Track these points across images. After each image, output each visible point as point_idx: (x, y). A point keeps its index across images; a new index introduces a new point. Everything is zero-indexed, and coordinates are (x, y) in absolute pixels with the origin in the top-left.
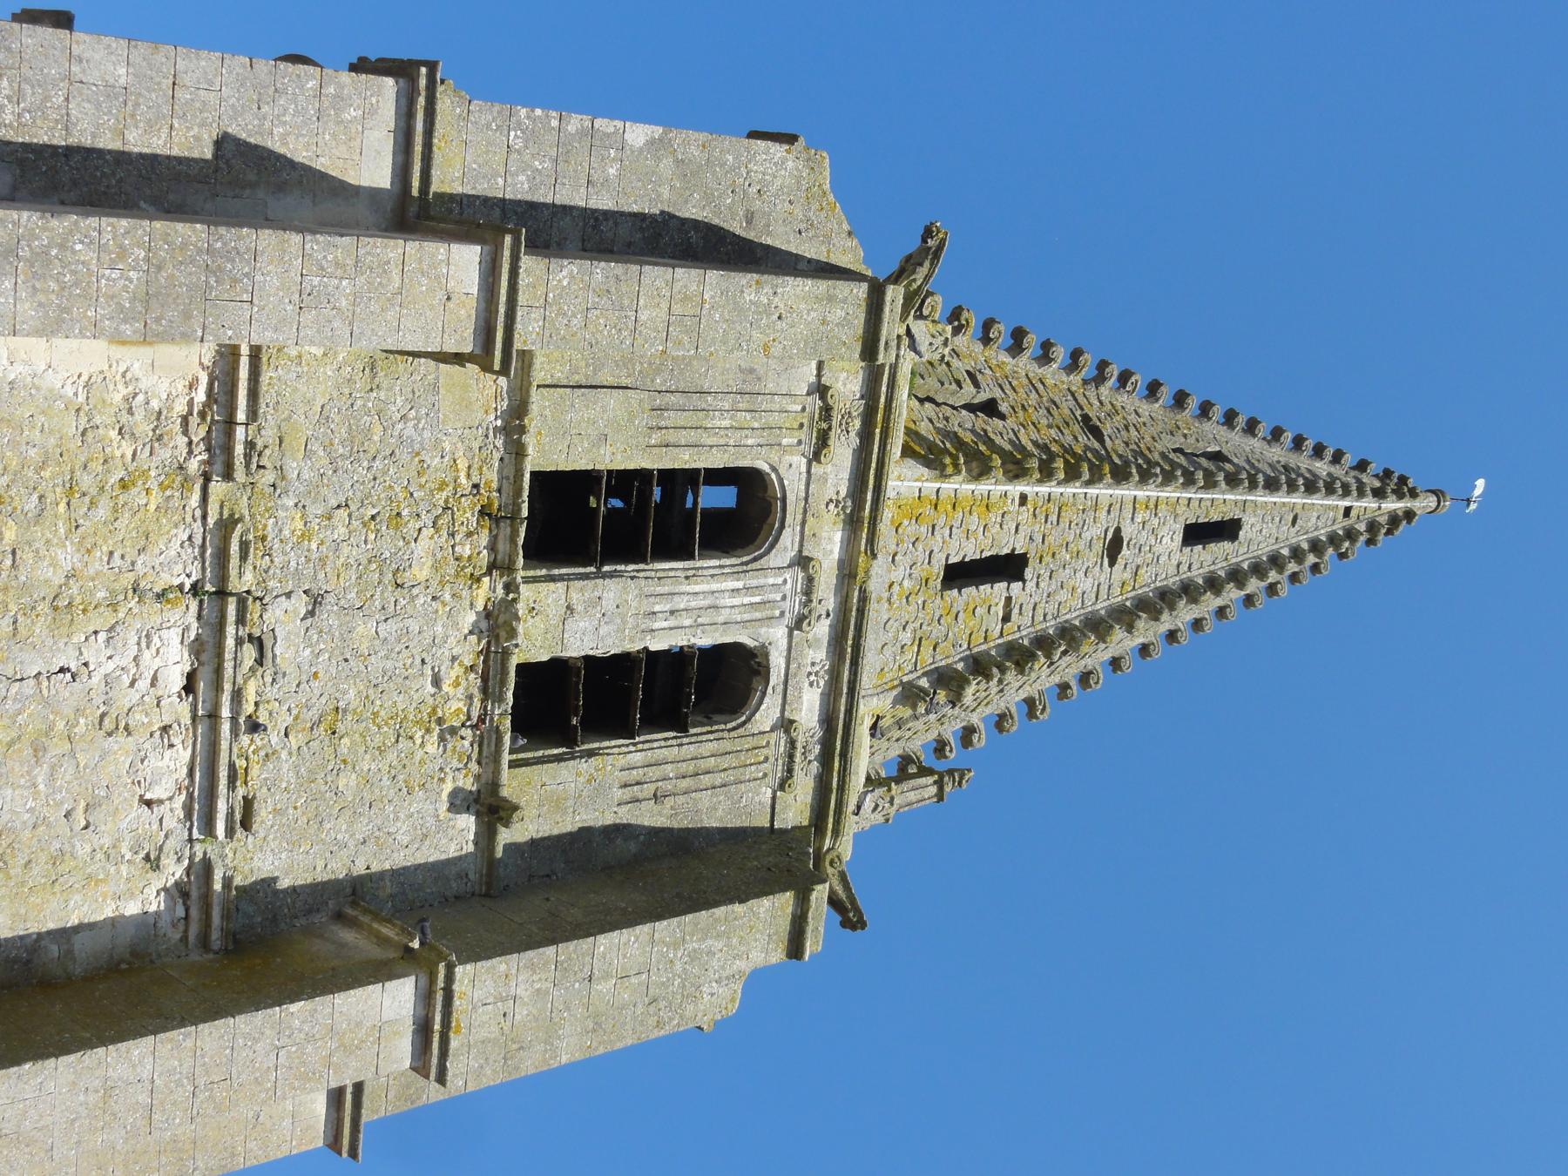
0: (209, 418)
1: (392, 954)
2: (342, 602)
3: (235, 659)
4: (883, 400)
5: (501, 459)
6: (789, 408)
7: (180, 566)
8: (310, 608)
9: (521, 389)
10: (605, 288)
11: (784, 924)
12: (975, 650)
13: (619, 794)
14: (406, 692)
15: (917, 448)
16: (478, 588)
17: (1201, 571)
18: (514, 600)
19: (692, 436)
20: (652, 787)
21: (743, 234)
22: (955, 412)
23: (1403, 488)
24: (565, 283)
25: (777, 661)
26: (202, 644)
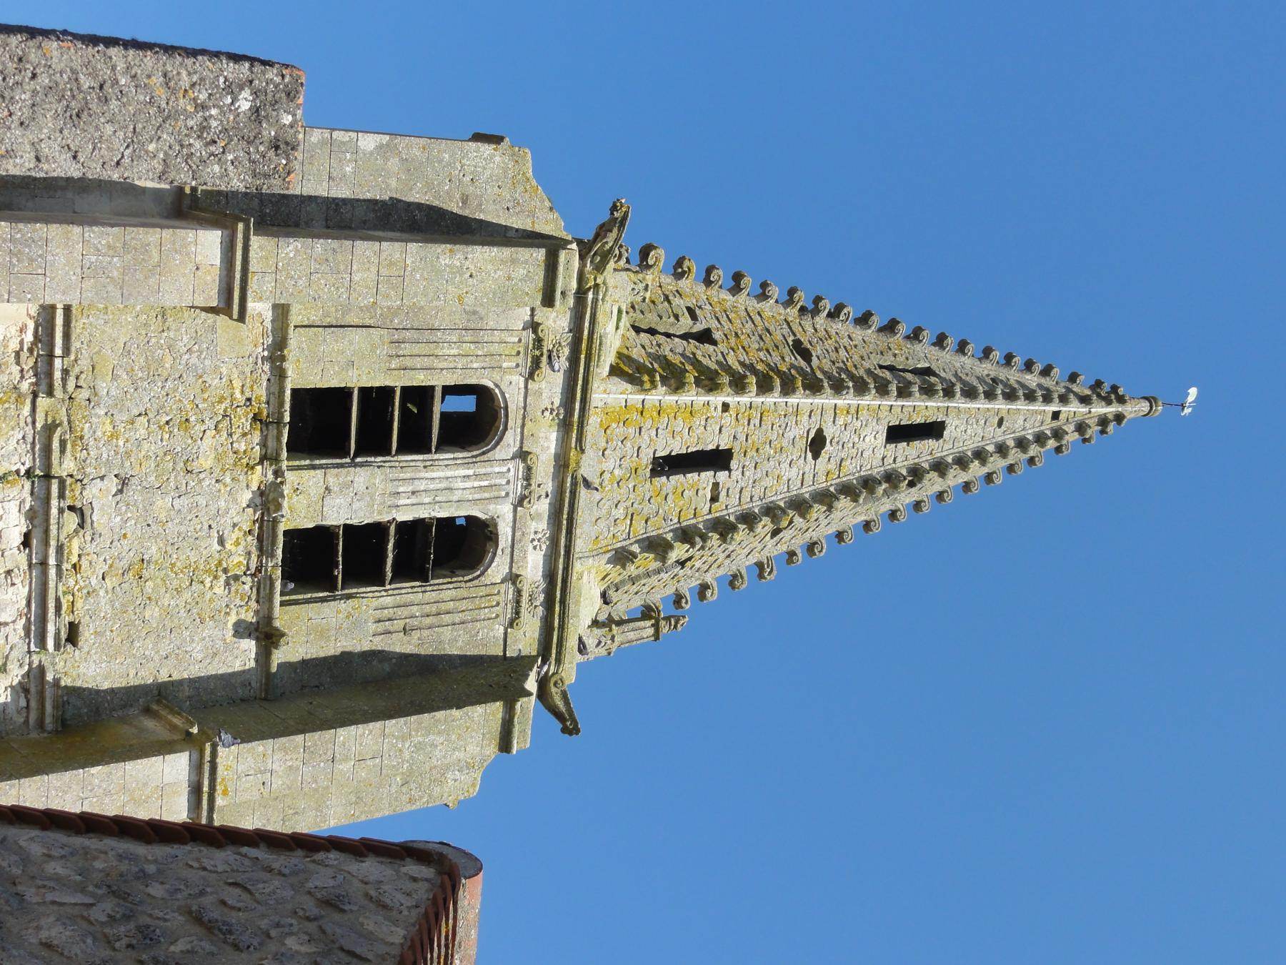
0: (35, 353)
1: (177, 737)
2: (145, 483)
3: (58, 523)
4: (586, 333)
5: (269, 380)
6: (508, 340)
7: (17, 457)
8: (120, 487)
9: (282, 329)
10: (325, 257)
11: (496, 726)
12: (685, 524)
13: (372, 627)
14: (196, 549)
15: (626, 369)
16: (252, 474)
17: (906, 463)
18: (282, 483)
19: (426, 362)
20: (402, 623)
21: (460, 212)
22: (668, 340)
23: (1115, 396)
24: (292, 255)
25: (504, 531)
26: (35, 512)
